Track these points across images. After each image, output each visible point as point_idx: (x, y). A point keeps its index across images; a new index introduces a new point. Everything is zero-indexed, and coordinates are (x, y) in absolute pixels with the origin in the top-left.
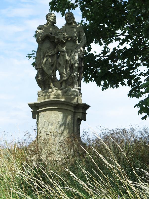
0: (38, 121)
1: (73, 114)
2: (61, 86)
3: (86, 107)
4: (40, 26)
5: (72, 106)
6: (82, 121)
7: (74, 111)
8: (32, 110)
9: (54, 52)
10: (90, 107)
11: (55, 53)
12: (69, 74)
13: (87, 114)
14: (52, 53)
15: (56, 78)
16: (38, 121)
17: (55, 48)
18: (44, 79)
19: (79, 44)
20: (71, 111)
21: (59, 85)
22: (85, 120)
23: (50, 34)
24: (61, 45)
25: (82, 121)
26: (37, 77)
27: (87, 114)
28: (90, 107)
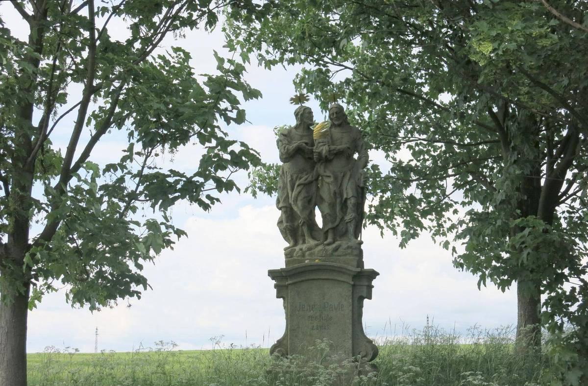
0: (453, 191)
1: (351, 289)
2: (326, 239)
3: (373, 274)
4: (118, 42)
5: (349, 275)
6: (366, 301)
7: (352, 283)
8: (274, 282)
9: (312, 177)
10: (378, 274)
11: (314, 179)
12: (341, 217)
13: (373, 287)
14: (308, 180)
15: (316, 225)
16: (453, 191)
17: (314, 169)
18: (294, 225)
19: (576, 294)
20: (347, 283)
21: (322, 236)
22: (370, 297)
23: (304, 144)
24: (324, 164)
25: (366, 301)
26: (280, 223)
27: (373, 287)
28: (378, 274)
